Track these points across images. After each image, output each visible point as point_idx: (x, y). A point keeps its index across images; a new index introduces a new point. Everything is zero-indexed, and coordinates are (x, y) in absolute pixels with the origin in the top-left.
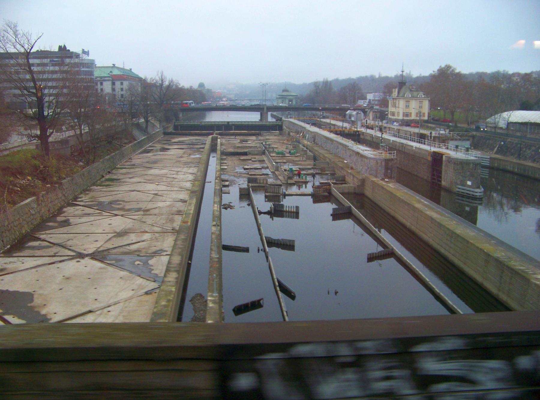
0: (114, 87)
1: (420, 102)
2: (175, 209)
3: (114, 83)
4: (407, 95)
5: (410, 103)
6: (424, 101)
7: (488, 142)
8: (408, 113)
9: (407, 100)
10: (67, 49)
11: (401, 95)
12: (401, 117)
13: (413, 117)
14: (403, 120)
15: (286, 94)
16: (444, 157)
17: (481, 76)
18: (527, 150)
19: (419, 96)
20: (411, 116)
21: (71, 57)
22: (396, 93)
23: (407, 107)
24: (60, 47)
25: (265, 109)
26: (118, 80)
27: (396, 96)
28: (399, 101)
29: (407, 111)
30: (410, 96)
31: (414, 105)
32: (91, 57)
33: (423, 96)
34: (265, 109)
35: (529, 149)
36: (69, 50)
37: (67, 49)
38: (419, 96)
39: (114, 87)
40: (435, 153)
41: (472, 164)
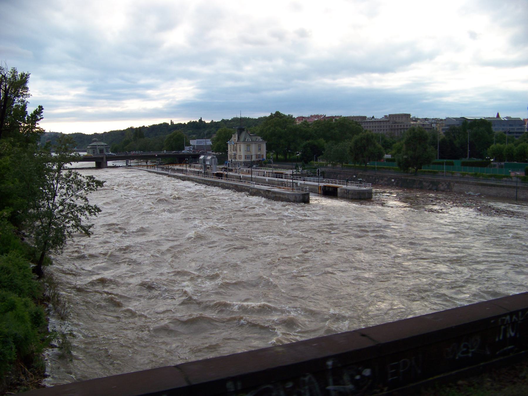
2: (428, 283)
5: (262, 146)
7: (339, 176)
9: (248, 144)
11: (242, 139)
12: (243, 160)
13: (254, 159)
14: (245, 162)
16: (339, 190)
17: (69, 134)
18: (380, 181)
22: (236, 138)
25: (105, 159)
27: (237, 140)
28: (240, 145)
29: (249, 153)
30: (250, 140)
31: (254, 148)
33: (261, 140)
34: (105, 159)
35: (382, 180)
40: (325, 186)
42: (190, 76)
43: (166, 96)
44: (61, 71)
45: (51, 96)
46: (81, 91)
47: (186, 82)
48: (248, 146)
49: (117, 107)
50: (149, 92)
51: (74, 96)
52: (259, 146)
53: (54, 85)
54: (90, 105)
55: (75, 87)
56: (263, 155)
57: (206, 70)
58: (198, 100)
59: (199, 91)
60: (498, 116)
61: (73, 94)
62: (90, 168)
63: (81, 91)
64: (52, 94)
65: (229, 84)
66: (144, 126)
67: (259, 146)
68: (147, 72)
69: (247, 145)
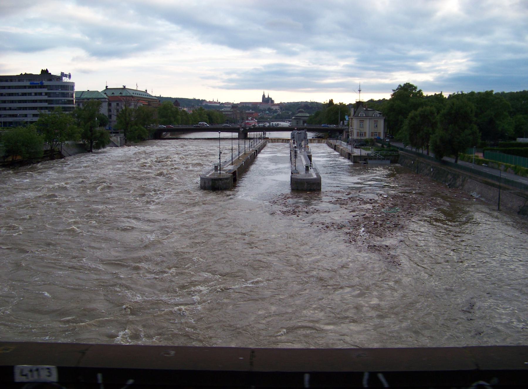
0: (110, 108)
1: (375, 121)
3: (111, 104)
4: (361, 114)
6: (379, 120)
8: (376, 132)
9: (376, 120)
10: (49, 72)
13: (367, 137)
15: (301, 115)
19: (373, 116)
20: (365, 136)
21: (50, 80)
23: (361, 126)
24: (42, 71)
26: (114, 101)
30: (364, 115)
32: (71, 80)
33: (378, 116)
36: (50, 73)
37: (49, 72)
38: (373, 116)
39: (110, 108)
41: (306, 184)
42: (464, 47)
43: (437, 68)
44: (331, 42)
45: (320, 66)
46: (349, 62)
47: (459, 54)
48: (362, 121)
49: (386, 78)
50: (420, 64)
51: (344, 66)
52: (376, 122)
53: (323, 55)
54: (358, 76)
55: (343, 57)
56: (380, 133)
57: (482, 41)
58: (472, 74)
59: (473, 64)
60: (160, 95)
61: (342, 64)
62: (232, 139)
63: (349, 62)
64: (321, 65)
65: (509, 56)
66: (384, 99)
67: (376, 122)
68: (418, 43)
69: (360, 121)
